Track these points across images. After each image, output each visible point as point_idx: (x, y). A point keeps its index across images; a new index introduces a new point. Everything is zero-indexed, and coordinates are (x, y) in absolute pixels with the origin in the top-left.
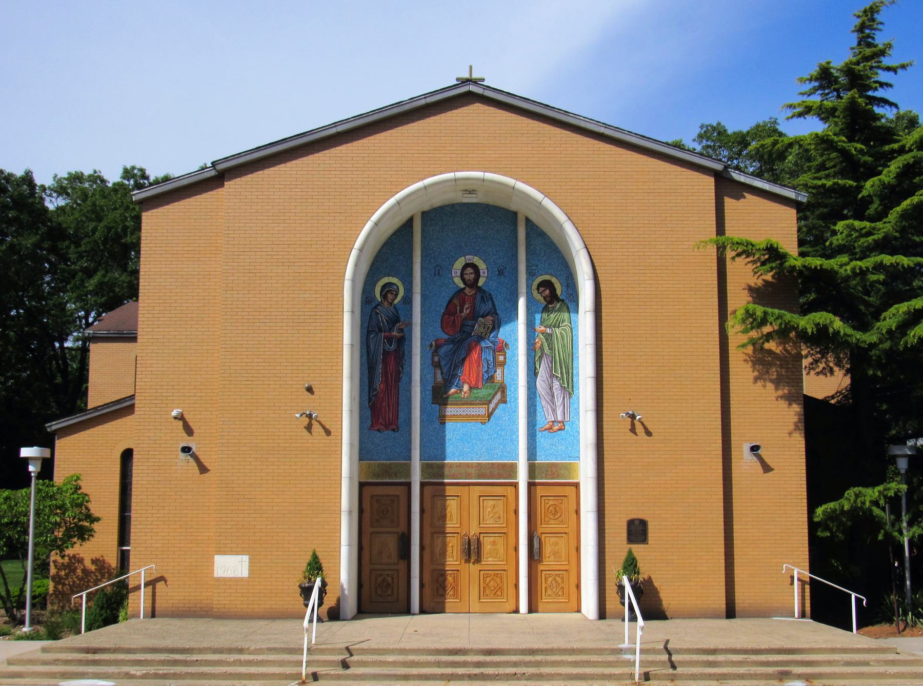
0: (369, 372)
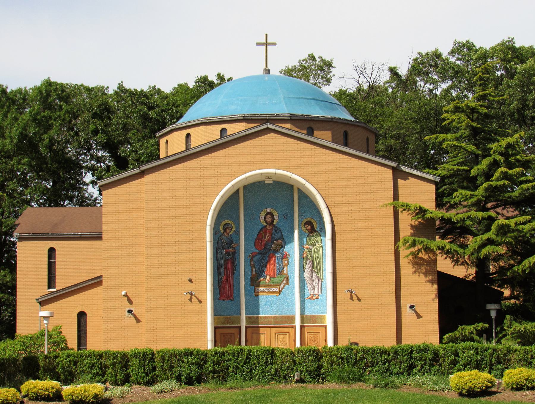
0: (218, 270)
